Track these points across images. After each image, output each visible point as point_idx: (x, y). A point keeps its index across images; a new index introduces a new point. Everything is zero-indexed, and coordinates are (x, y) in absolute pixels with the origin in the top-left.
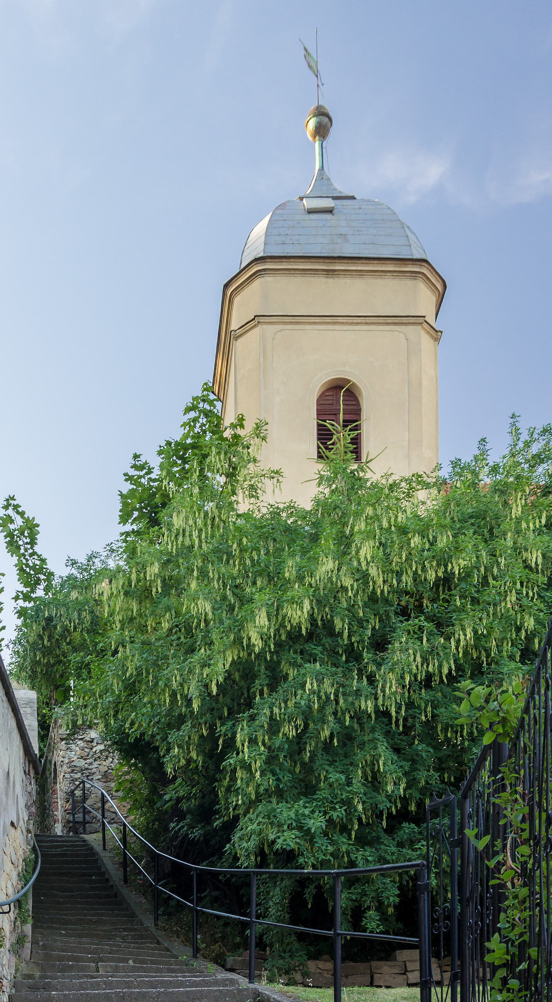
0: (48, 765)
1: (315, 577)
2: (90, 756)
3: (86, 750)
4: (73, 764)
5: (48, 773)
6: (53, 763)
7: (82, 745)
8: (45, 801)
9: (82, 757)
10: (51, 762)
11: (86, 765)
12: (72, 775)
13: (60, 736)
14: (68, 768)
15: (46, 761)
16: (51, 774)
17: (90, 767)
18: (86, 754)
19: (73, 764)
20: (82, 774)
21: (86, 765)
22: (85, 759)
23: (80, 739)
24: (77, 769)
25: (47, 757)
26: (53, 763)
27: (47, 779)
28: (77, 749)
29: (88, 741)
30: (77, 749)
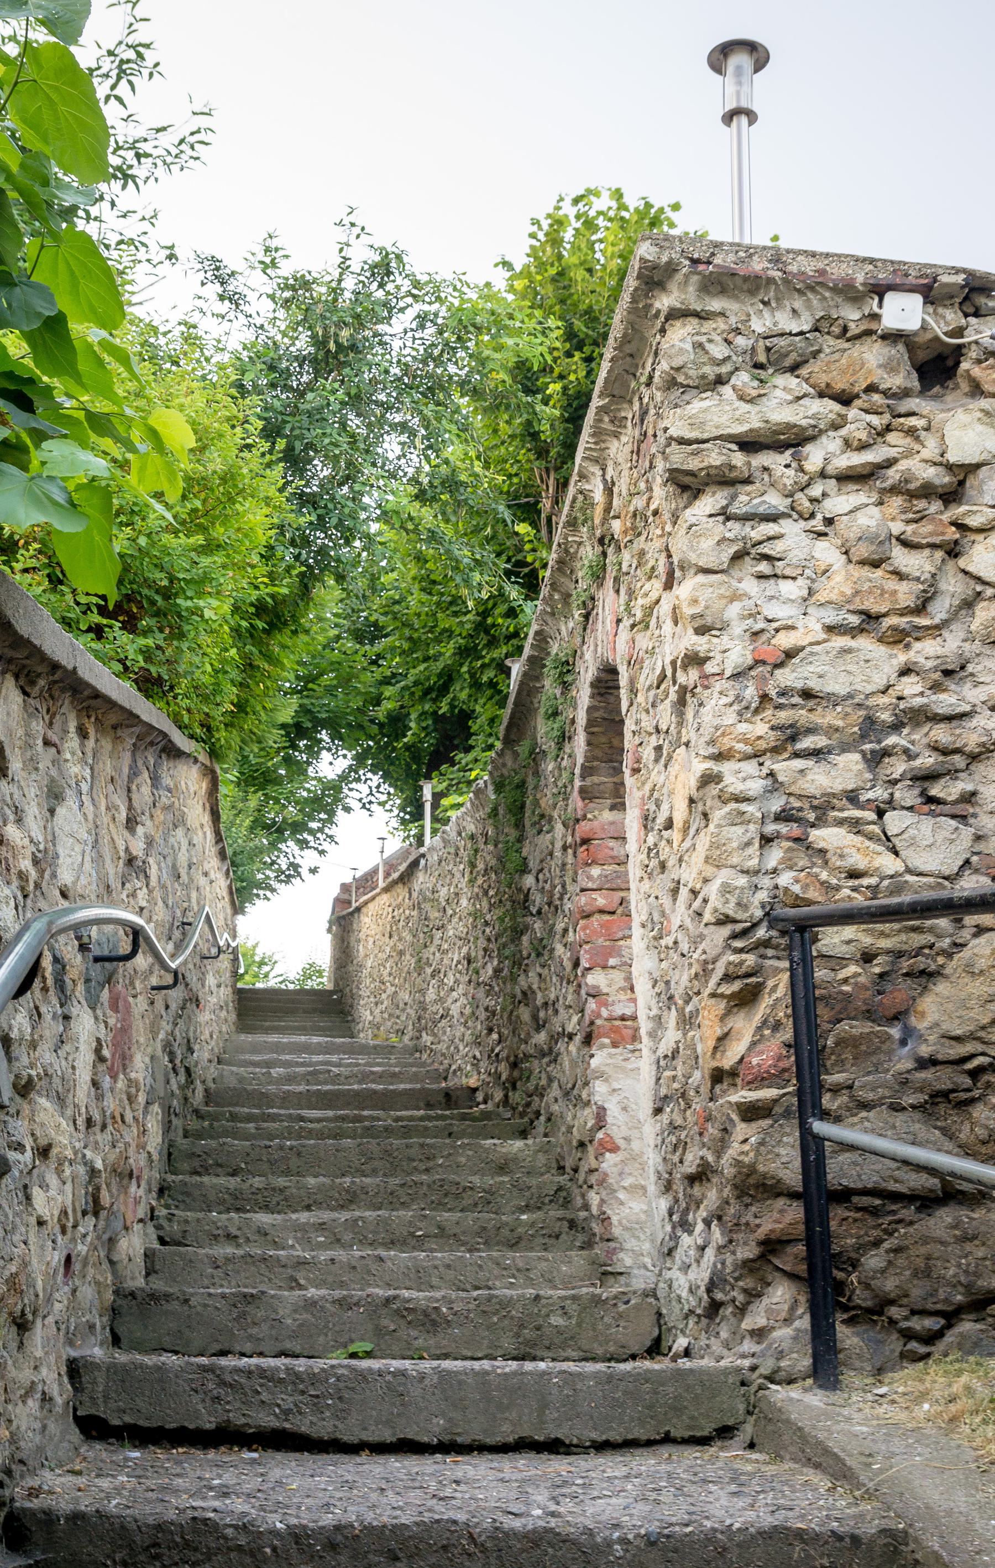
0: (549, 685)
1: (168, 867)
2: (939, 610)
3: (902, 558)
4: (788, 677)
5: (543, 729)
6: (587, 672)
7: (870, 519)
8: (524, 869)
9: (870, 618)
10: (567, 668)
11: (911, 687)
12: (785, 768)
13: (679, 458)
14: (748, 712)
15: (536, 663)
16: (564, 738)
17: (946, 702)
18: (906, 594)
19: (788, 677)
20: (876, 759)
21: (911, 687)
22: (899, 638)
23: (847, 478)
24: (828, 717)
25: (542, 638)
26: (587, 672)
27: (536, 756)
28: (827, 552)
29: (927, 491)
30: (827, 552)
